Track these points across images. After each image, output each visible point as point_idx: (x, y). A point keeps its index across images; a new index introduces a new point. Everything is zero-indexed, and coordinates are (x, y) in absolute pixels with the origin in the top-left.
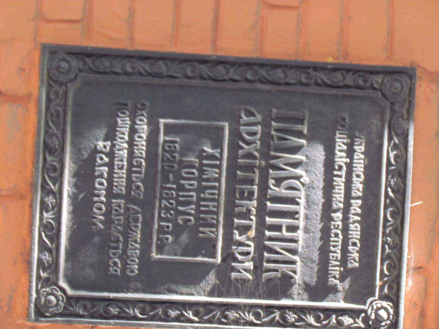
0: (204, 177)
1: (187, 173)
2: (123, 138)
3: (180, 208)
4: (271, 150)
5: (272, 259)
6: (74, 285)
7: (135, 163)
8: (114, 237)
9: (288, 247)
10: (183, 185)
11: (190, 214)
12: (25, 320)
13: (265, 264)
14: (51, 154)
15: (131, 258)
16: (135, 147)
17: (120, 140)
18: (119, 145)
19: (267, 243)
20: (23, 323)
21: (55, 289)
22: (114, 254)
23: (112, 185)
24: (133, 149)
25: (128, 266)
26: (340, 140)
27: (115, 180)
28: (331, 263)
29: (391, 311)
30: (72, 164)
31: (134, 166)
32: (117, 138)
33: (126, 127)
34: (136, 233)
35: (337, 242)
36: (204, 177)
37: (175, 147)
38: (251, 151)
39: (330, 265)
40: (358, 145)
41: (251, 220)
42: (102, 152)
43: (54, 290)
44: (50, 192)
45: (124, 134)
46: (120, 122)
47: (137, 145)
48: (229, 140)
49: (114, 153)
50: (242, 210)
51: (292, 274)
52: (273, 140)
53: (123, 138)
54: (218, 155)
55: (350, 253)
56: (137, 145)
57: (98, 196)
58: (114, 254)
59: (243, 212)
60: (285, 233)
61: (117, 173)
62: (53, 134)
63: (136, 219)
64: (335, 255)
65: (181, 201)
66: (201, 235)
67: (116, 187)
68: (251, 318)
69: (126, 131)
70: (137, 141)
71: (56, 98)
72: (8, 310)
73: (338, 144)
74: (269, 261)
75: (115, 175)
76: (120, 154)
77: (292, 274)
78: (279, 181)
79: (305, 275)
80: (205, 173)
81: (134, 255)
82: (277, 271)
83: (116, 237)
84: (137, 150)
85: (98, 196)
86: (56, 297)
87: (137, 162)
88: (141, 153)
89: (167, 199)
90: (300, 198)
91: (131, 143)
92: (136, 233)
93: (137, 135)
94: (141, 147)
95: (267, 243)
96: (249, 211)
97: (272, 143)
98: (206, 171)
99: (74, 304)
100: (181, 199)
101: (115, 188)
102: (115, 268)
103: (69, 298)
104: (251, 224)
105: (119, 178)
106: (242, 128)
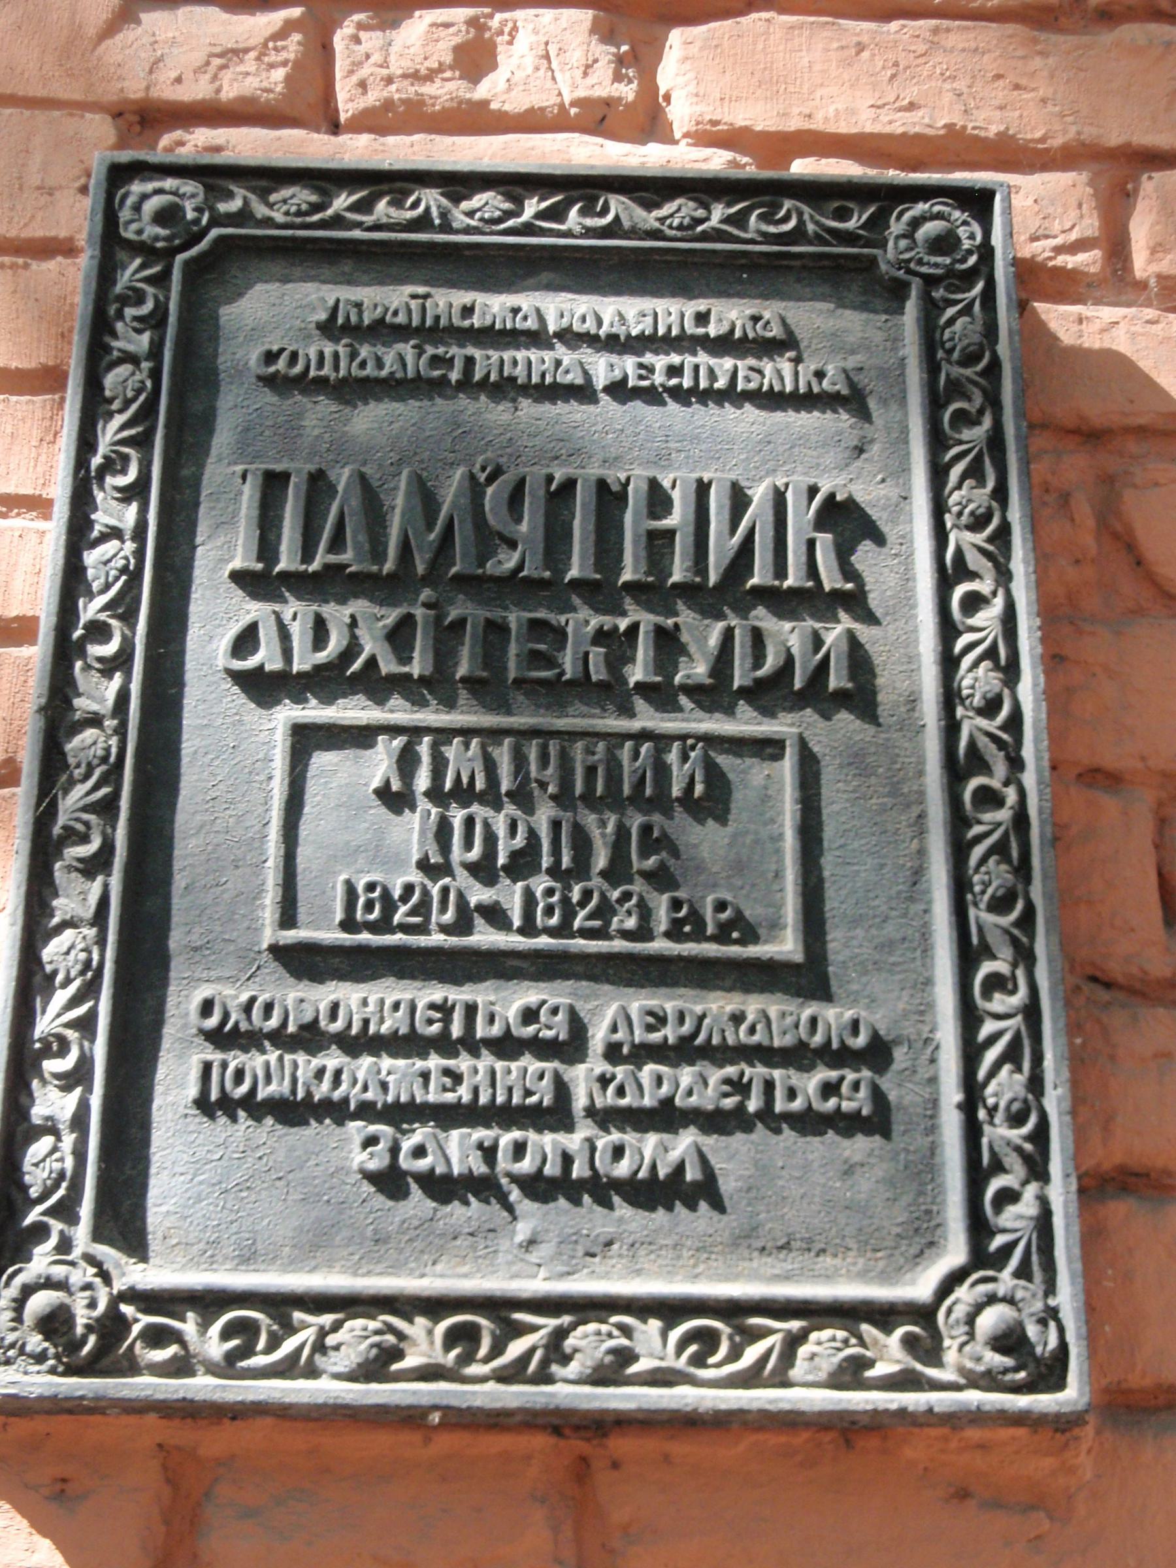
0: (480, 785)
1: (468, 844)
2: (338, 1073)
3: (601, 861)
4: (381, 570)
5: (770, 556)
6: (923, 1237)
7: (436, 1028)
8: (726, 1095)
9: (726, 515)
10: (514, 855)
11: (622, 833)
12: (1077, 1439)
13: (789, 582)
14: (397, 1354)
15: (803, 1032)
16: (372, 1029)
17: (344, 1087)
18: (365, 1088)
19: (713, 578)
20: (1089, 1452)
21: (949, 1311)
22: (792, 1094)
23: (523, 1109)
24: (378, 1037)
25: (835, 1045)
26: (343, 364)
27: (500, 1099)
28: (771, 387)
29: (921, 207)
30: (439, 1268)
31: (446, 1031)
32: (337, 1095)
33: (295, 1065)
34: (702, 1018)
35: (696, 368)
36: (480, 785)
37: (371, 887)
38: (380, 634)
39: (777, 388)
40: (360, 314)
41: (634, 628)
42: (395, 1150)
43: (953, 1316)
44: (556, 1349)
45: (320, 1073)
46: (273, 1088)
47: (366, 1022)
48: (326, 521)
49: (397, 1103)
50: (602, 658)
51: (818, 499)
52: (342, 567)
53: (338, 1073)
54: (398, 742)
55: (732, 331)
56: (366, 1022)
57: (567, 1159)
58: (792, 1094)
59: (606, 655)
60: (677, 517)
61: (476, 1091)
62: (320, 1347)
63: (650, 1020)
64: (740, 375)
65: (574, 859)
66: (699, 789)
67: (528, 1093)
68: (988, 617)
69: (305, 1063)
70: (349, 1026)
71: (177, 1337)
72: (1042, 1514)
73: (355, 371)
74: (781, 571)
75: (483, 1099)
76: (399, 1083)
77: (818, 499)
78: (489, 540)
79: (818, 465)
80: (465, 780)
81: (789, 1020)
82: (811, 544)
83: (726, 1088)
84: (382, 1021)
85: (567, 1159)
86: (978, 1308)
87: (430, 1022)
88: (396, 1006)
89: (569, 913)
90: (550, 479)
91: (358, 1043)
92: (702, 1018)
93: (323, 1023)
94: (371, 1008)
95: (713, 578)
96: (601, 637)
97: (352, 569)
98: (458, 779)
99: (999, 1241)
100: (566, 862)
101: (533, 1099)
102: (845, 1089)
103: (983, 1258)
104: (651, 628)
105: (493, 1085)
106: (296, 668)
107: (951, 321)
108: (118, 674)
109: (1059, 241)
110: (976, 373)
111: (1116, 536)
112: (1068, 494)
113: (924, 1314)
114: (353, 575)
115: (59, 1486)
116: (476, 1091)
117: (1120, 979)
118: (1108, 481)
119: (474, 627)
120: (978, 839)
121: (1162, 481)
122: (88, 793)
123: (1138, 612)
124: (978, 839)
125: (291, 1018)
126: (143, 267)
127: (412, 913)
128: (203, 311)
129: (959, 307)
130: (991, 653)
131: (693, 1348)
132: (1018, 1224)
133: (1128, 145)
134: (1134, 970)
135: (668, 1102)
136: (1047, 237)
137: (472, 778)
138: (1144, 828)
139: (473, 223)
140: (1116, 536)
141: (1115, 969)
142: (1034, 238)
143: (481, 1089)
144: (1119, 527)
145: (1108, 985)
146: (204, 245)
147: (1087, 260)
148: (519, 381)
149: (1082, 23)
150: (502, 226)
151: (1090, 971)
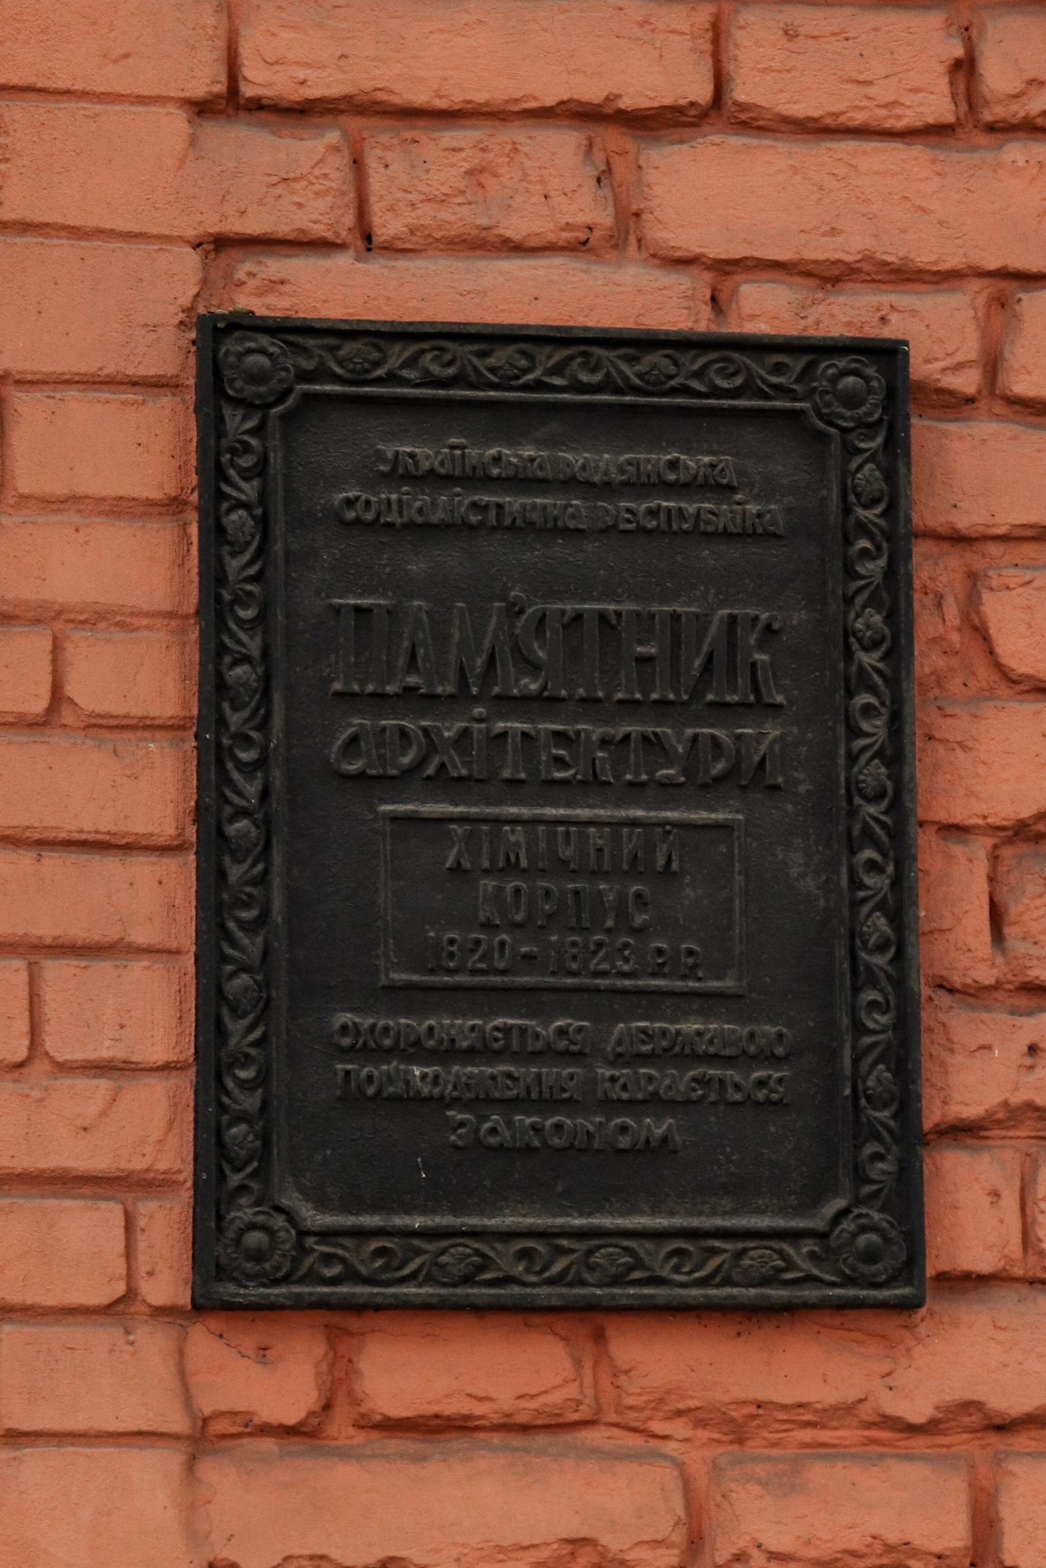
29: (842, 363)
42: (477, 1130)
46: (391, 1089)
55: (696, 478)
61: (528, 1089)
80: (513, 859)
97: (422, 691)
107: (860, 468)
108: (259, 774)
109: (942, 364)
110: (876, 515)
111: (975, 629)
112: (942, 597)
113: (821, 1236)
114: (423, 696)
115: (262, 1352)
116: (528, 1089)
117: (958, 986)
118: (973, 577)
119: (514, 738)
120: (864, 900)
121: (1012, 586)
122: (246, 872)
123: (988, 695)
124: (864, 900)
125: (402, 1039)
126: (245, 418)
127: (481, 959)
128: (193, 335)
129: (868, 454)
130: (879, 754)
131: (674, 1260)
132: (882, 1178)
133: (1005, 267)
134: (969, 981)
135: (655, 1094)
136: (937, 359)
137: (517, 858)
138: (982, 868)
139: (495, 379)
140: (975, 629)
141: (957, 980)
142: (928, 361)
143: (532, 1089)
144: (977, 622)
145: (951, 991)
146: (290, 401)
147: (967, 382)
148: (538, 526)
149: (975, 131)
150: (521, 381)
151: (939, 981)
